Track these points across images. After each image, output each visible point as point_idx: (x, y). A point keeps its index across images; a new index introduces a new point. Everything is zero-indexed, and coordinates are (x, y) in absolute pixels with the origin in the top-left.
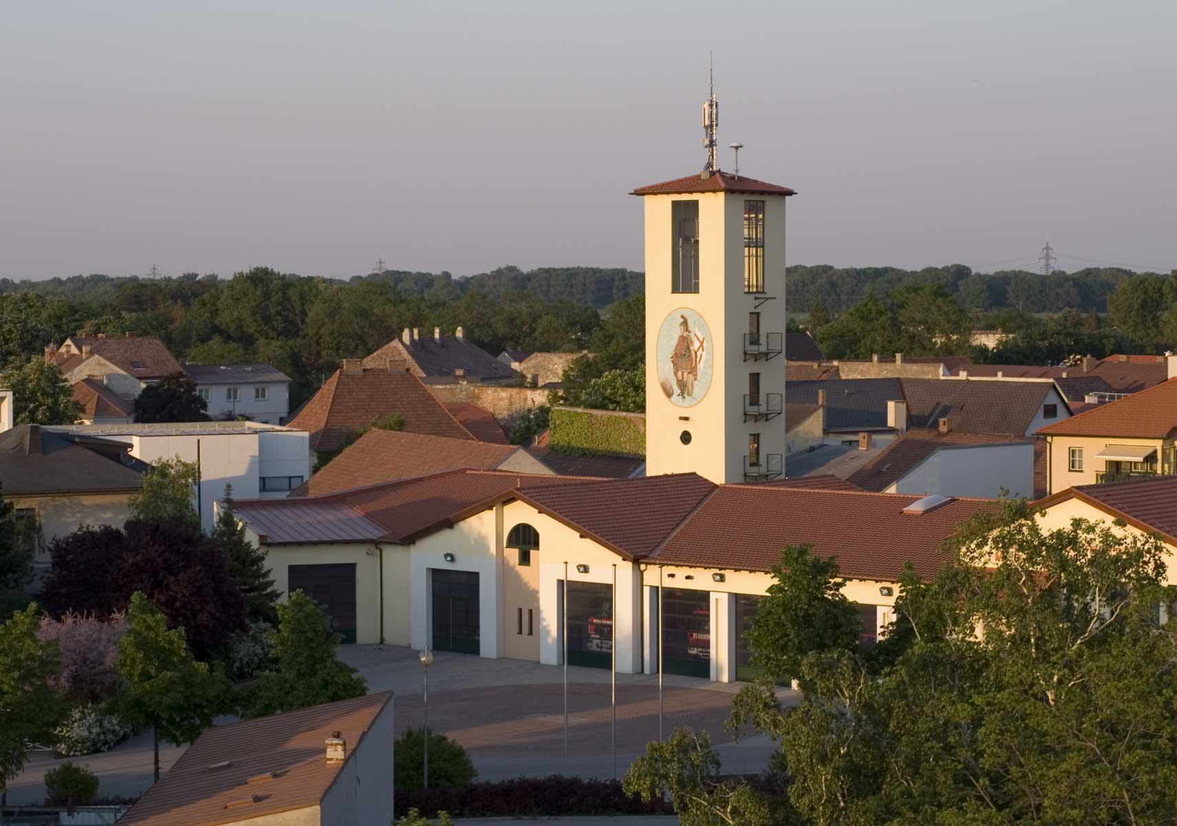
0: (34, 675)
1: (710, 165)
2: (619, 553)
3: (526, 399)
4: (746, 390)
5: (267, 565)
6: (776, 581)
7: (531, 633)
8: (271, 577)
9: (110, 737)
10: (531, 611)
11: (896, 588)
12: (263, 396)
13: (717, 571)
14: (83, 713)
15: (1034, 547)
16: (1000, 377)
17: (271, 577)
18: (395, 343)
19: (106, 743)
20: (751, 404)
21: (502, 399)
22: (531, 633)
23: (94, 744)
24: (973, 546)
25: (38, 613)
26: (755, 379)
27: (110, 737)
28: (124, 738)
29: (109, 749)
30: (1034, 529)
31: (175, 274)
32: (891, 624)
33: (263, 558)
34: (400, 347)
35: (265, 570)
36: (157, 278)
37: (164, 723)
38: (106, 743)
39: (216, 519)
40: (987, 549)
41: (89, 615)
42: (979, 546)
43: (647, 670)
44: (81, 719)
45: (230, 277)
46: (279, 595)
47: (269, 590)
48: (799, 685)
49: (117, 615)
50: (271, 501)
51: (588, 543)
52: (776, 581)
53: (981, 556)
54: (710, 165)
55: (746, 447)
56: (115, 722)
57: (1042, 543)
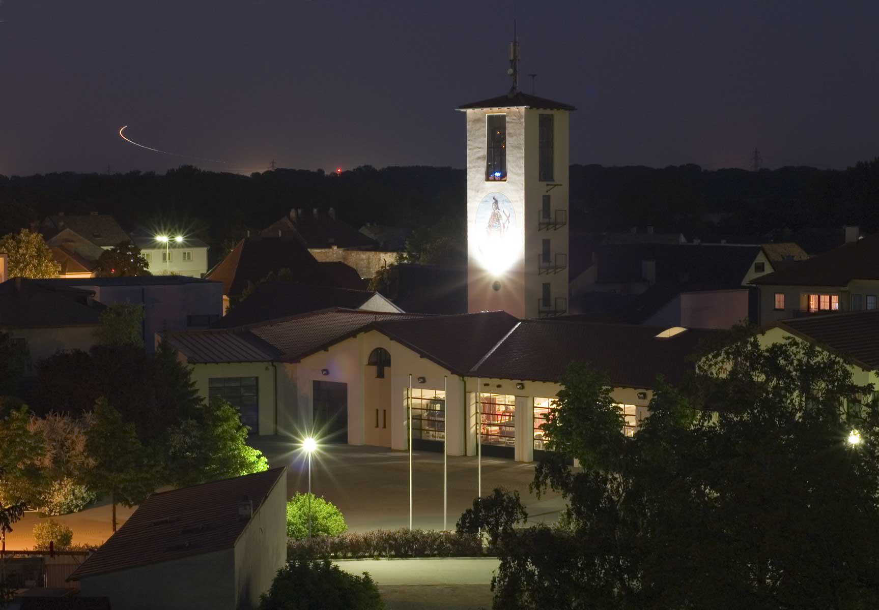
0: (26, 457)
1: (514, 88)
2: (449, 369)
3: (380, 260)
4: (541, 206)
5: (193, 378)
6: (563, 388)
7: (385, 427)
8: (196, 387)
9: (80, 502)
10: (385, 411)
11: (650, 394)
12: (189, 258)
13: (520, 381)
14: (60, 484)
15: (755, 358)
16: (723, 243)
17: (196, 387)
18: (285, 220)
19: (77, 506)
20: (544, 305)
21: (362, 260)
22: (385, 427)
23: (69, 507)
24: (710, 356)
25: (28, 412)
26: (546, 243)
27: (80, 502)
28: (91, 502)
29: (80, 510)
30: (755, 345)
31: (124, 171)
32: (647, 419)
33: (190, 373)
34: (290, 224)
35: (192, 381)
36: (111, 173)
37: (120, 491)
38: (77, 506)
39: (156, 344)
40: (720, 358)
41: (65, 414)
42: (715, 357)
43: (469, 453)
44: (59, 489)
45: (164, 173)
46: (202, 400)
47: (195, 396)
48: (580, 463)
49: (86, 415)
50: (421, 553)
51: (425, 361)
52: (563, 388)
53: (716, 363)
54: (514, 88)
55: (540, 249)
56: (83, 491)
57: (761, 355)
